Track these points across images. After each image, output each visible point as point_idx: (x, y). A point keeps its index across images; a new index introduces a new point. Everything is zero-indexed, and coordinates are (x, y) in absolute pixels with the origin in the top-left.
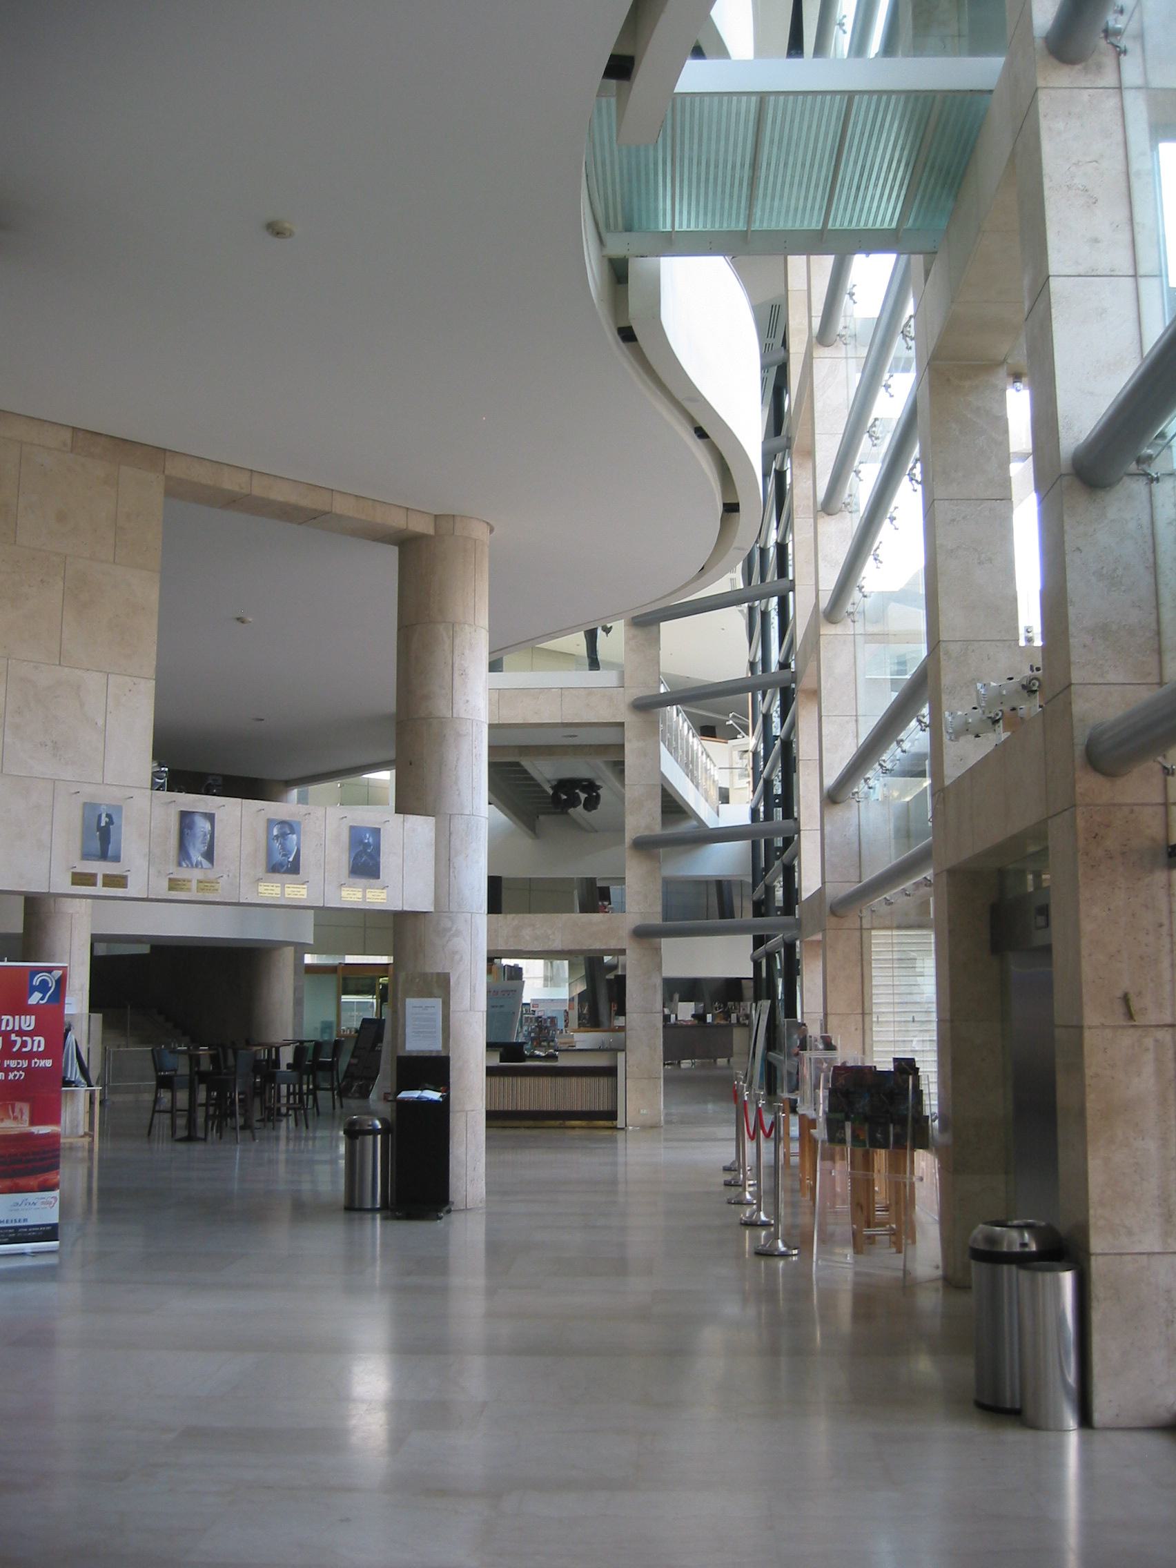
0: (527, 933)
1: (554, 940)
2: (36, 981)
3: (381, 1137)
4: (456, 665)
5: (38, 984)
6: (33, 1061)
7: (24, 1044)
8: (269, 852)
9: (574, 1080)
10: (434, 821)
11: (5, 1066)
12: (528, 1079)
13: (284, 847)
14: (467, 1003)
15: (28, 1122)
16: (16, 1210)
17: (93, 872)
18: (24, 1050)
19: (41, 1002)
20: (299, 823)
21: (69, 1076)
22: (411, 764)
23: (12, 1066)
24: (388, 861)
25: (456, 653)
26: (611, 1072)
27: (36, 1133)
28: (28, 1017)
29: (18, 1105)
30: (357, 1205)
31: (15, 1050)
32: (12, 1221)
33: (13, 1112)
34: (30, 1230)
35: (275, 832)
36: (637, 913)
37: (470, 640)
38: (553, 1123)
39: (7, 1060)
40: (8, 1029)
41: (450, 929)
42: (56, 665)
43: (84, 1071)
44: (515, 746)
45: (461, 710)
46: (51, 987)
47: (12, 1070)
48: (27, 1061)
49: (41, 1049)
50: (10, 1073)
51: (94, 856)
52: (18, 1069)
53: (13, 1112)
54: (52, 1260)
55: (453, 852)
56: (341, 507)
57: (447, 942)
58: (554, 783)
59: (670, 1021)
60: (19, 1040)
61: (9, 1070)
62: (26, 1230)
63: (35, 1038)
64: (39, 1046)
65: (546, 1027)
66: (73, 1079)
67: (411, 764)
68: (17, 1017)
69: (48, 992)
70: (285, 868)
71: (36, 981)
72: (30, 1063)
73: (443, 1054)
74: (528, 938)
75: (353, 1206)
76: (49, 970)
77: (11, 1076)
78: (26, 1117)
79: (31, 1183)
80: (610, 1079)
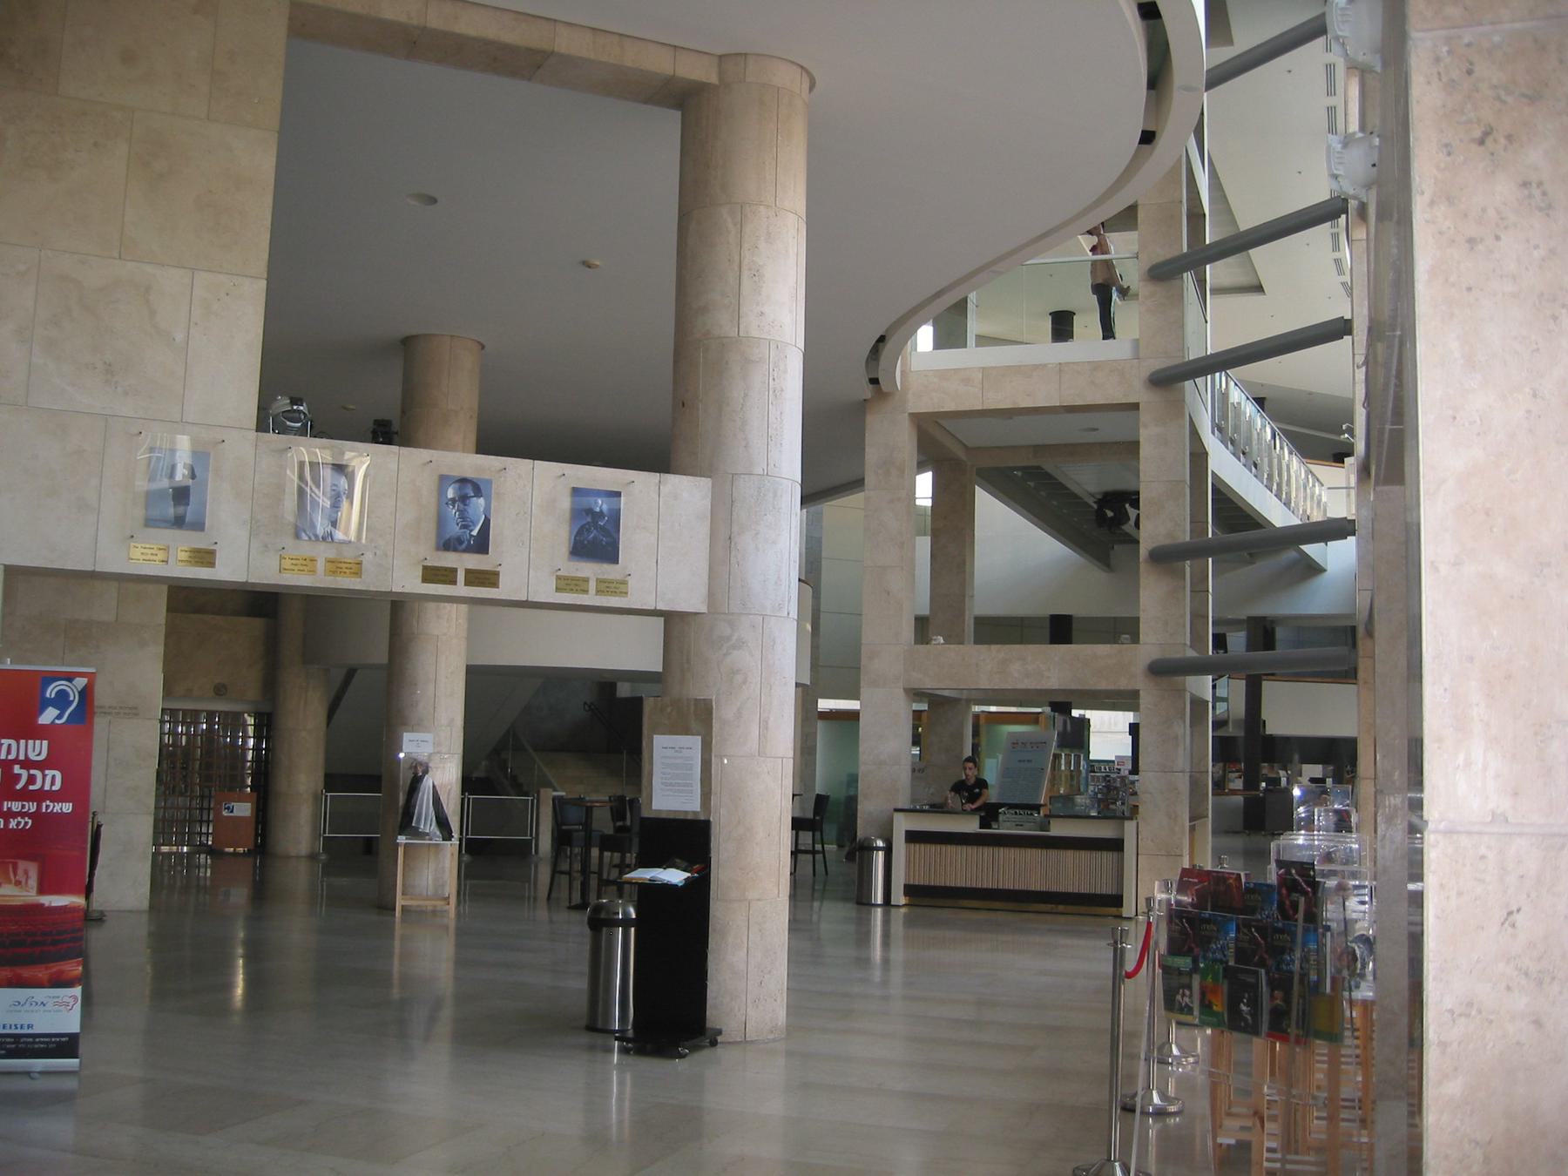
0: (1015, 668)
1: (1049, 677)
2: (51, 692)
3: (635, 930)
4: (745, 262)
5: (53, 696)
6: (44, 804)
7: (32, 780)
8: (441, 522)
9: (1070, 853)
10: (710, 484)
11: (5, 809)
12: (1012, 850)
13: (463, 515)
14: (753, 744)
15: (35, 889)
16: (16, 1011)
17: (425, 584)
18: (31, 788)
19: (57, 722)
20: (489, 482)
21: (422, 827)
22: (683, 405)
23: (14, 809)
24: (632, 540)
25: (746, 246)
26: (1116, 845)
27: (47, 904)
28: (38, 742)
29: (22, 865)
30: (600, 1025)
31: (19, 787)
32: (11, 1028)
33: (15, 874)
34: (37, 1040)
35: (450, 494)
36: (1153, 644)
37: (768, 227)
38: (1043, 907)
39: (8, 800)
40: (10, 757)
41: (729, 638)
42: (115, 258)
43: (443, 823)
44: (1029, 446)
45: (751, 325)
46: (73, 701)
47: (15, 815)
48: (35, 804)
49: (57, 787)
50: (11, 820)
51: (165, 521)
52: (23, 815)
53: (15, 874)
54: (70, 1084)
55: (735, 528)
56: (566, 43)
57: (725, 655)
58: (1100, 497)
59: (1280, 785)
60: (24, 774)
61: (11, 814)
62: (31, 1040)
63: (47, 772)
64: (53, 783)
65: (1116, 788)
66: (428, 831)
67: (683, 405)
68: (22, 742)
69: (68, 708)
70: (464, 546)
71: (51, 692)
72: (39, 807)
73: (702, 818)
74: (1016, 675)
75: (595, 1025)
76: (69, 677)
77: (13, 824)
78: (33, 882)
79: (40, 975)
80: (1115, 854)
